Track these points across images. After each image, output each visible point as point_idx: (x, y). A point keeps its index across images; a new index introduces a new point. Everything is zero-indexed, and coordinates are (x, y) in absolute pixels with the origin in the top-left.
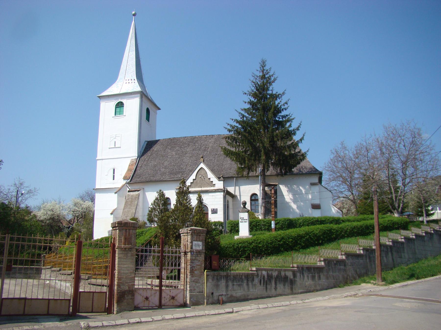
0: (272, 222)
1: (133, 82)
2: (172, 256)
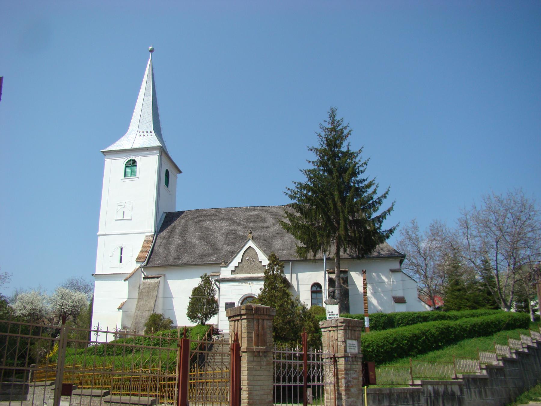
0: (366, 318)
1: (149, 135)
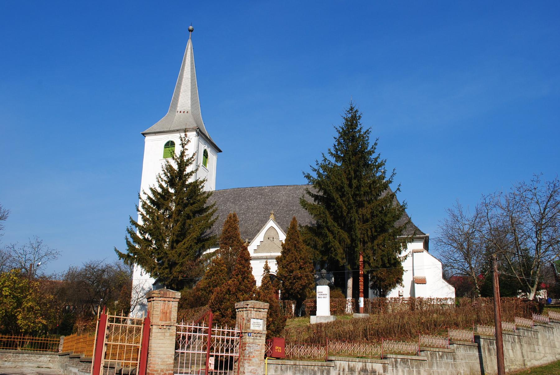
2: (223, 340)
